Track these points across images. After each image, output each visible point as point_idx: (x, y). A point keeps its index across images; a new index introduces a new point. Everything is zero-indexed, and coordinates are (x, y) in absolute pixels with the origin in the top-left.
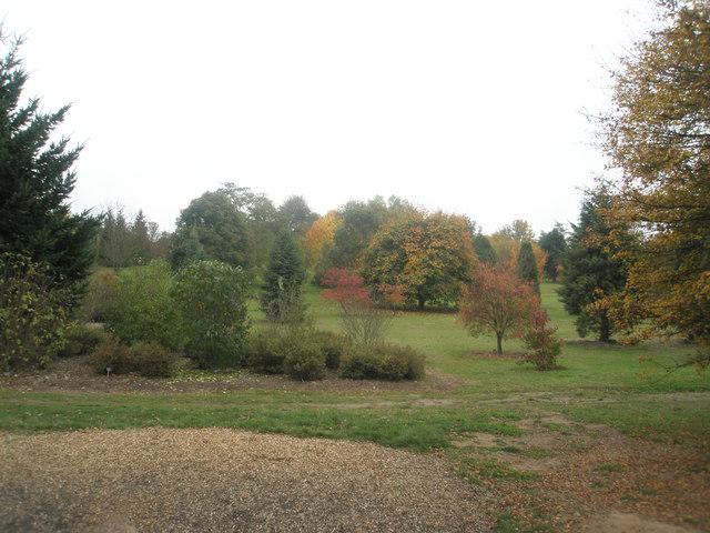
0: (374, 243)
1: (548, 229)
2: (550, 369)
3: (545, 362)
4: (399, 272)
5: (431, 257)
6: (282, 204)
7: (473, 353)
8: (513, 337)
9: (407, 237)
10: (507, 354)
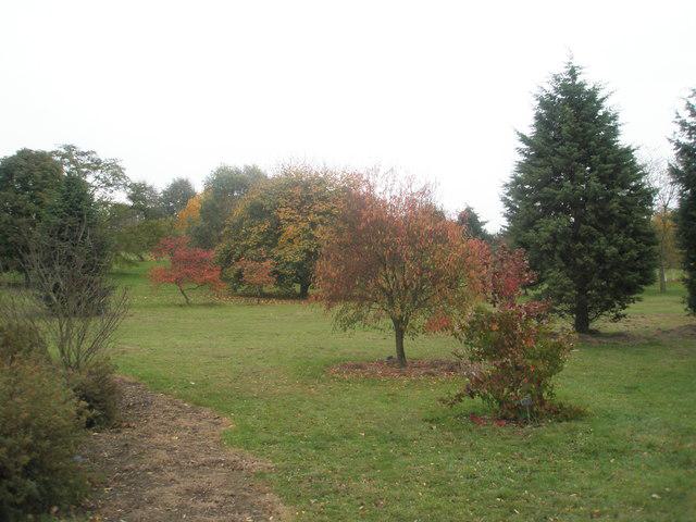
0: (238, 211)
1: (462, 208)
2: (536, 417)
3: (525, 400)
4: (271, 246)
5: (313, 225)
6: (165, 188)
7: (344, 366)
8: (429, 328)
9: (281, 200)
10: (418, 364)
